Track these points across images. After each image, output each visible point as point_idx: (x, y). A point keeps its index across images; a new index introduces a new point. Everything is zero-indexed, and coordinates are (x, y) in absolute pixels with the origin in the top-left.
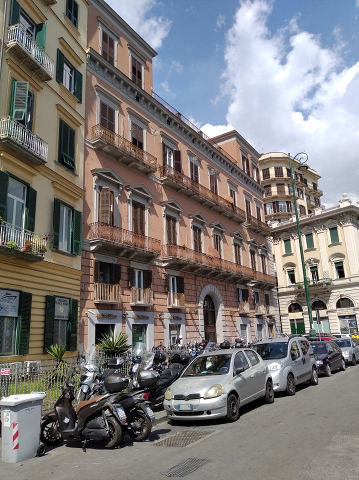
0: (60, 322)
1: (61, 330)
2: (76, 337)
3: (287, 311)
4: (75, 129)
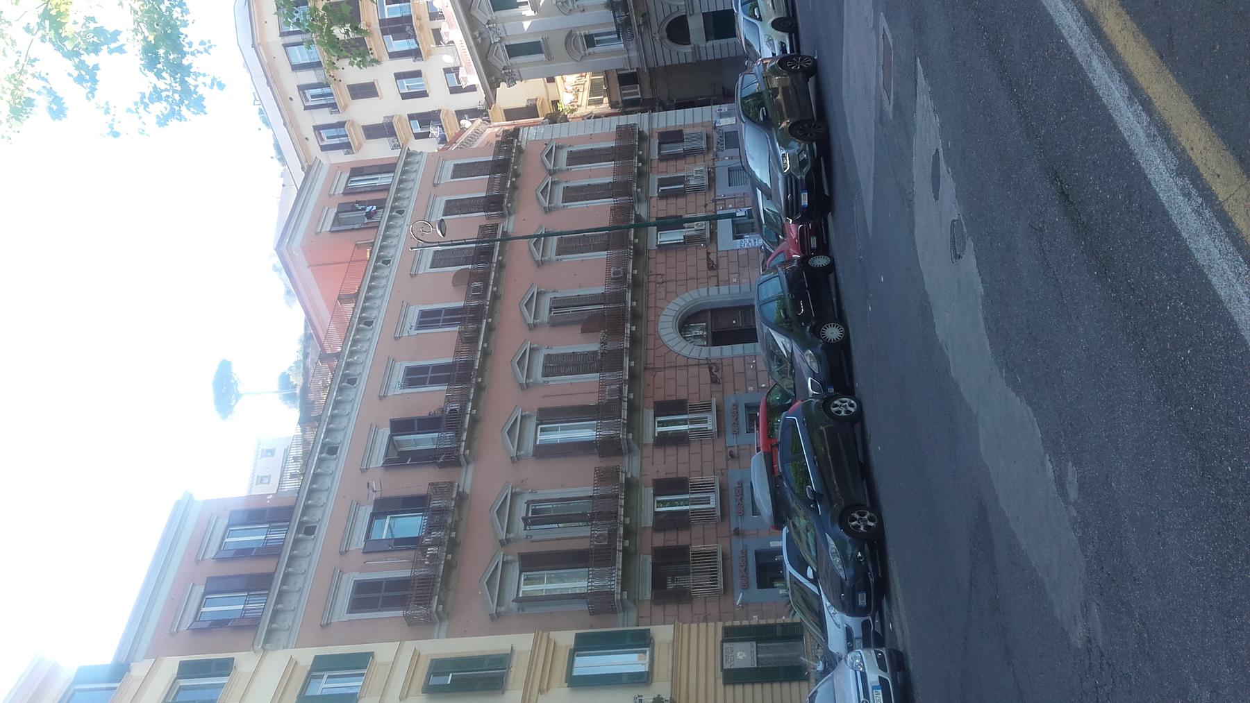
0: (759, 656)
1: (776, 653)
2: (782, 625)
3: (687, 49)
4: (429, 662)
